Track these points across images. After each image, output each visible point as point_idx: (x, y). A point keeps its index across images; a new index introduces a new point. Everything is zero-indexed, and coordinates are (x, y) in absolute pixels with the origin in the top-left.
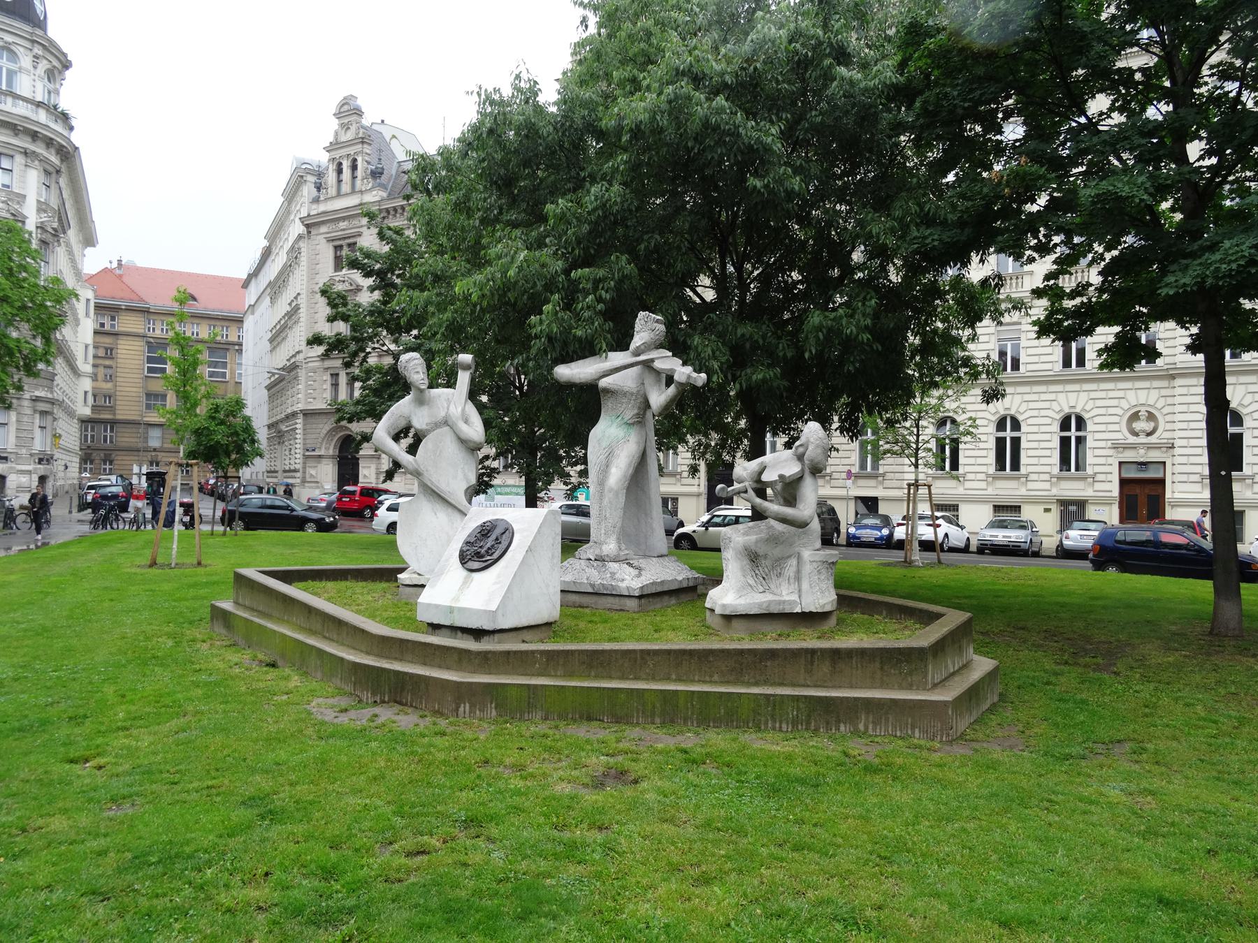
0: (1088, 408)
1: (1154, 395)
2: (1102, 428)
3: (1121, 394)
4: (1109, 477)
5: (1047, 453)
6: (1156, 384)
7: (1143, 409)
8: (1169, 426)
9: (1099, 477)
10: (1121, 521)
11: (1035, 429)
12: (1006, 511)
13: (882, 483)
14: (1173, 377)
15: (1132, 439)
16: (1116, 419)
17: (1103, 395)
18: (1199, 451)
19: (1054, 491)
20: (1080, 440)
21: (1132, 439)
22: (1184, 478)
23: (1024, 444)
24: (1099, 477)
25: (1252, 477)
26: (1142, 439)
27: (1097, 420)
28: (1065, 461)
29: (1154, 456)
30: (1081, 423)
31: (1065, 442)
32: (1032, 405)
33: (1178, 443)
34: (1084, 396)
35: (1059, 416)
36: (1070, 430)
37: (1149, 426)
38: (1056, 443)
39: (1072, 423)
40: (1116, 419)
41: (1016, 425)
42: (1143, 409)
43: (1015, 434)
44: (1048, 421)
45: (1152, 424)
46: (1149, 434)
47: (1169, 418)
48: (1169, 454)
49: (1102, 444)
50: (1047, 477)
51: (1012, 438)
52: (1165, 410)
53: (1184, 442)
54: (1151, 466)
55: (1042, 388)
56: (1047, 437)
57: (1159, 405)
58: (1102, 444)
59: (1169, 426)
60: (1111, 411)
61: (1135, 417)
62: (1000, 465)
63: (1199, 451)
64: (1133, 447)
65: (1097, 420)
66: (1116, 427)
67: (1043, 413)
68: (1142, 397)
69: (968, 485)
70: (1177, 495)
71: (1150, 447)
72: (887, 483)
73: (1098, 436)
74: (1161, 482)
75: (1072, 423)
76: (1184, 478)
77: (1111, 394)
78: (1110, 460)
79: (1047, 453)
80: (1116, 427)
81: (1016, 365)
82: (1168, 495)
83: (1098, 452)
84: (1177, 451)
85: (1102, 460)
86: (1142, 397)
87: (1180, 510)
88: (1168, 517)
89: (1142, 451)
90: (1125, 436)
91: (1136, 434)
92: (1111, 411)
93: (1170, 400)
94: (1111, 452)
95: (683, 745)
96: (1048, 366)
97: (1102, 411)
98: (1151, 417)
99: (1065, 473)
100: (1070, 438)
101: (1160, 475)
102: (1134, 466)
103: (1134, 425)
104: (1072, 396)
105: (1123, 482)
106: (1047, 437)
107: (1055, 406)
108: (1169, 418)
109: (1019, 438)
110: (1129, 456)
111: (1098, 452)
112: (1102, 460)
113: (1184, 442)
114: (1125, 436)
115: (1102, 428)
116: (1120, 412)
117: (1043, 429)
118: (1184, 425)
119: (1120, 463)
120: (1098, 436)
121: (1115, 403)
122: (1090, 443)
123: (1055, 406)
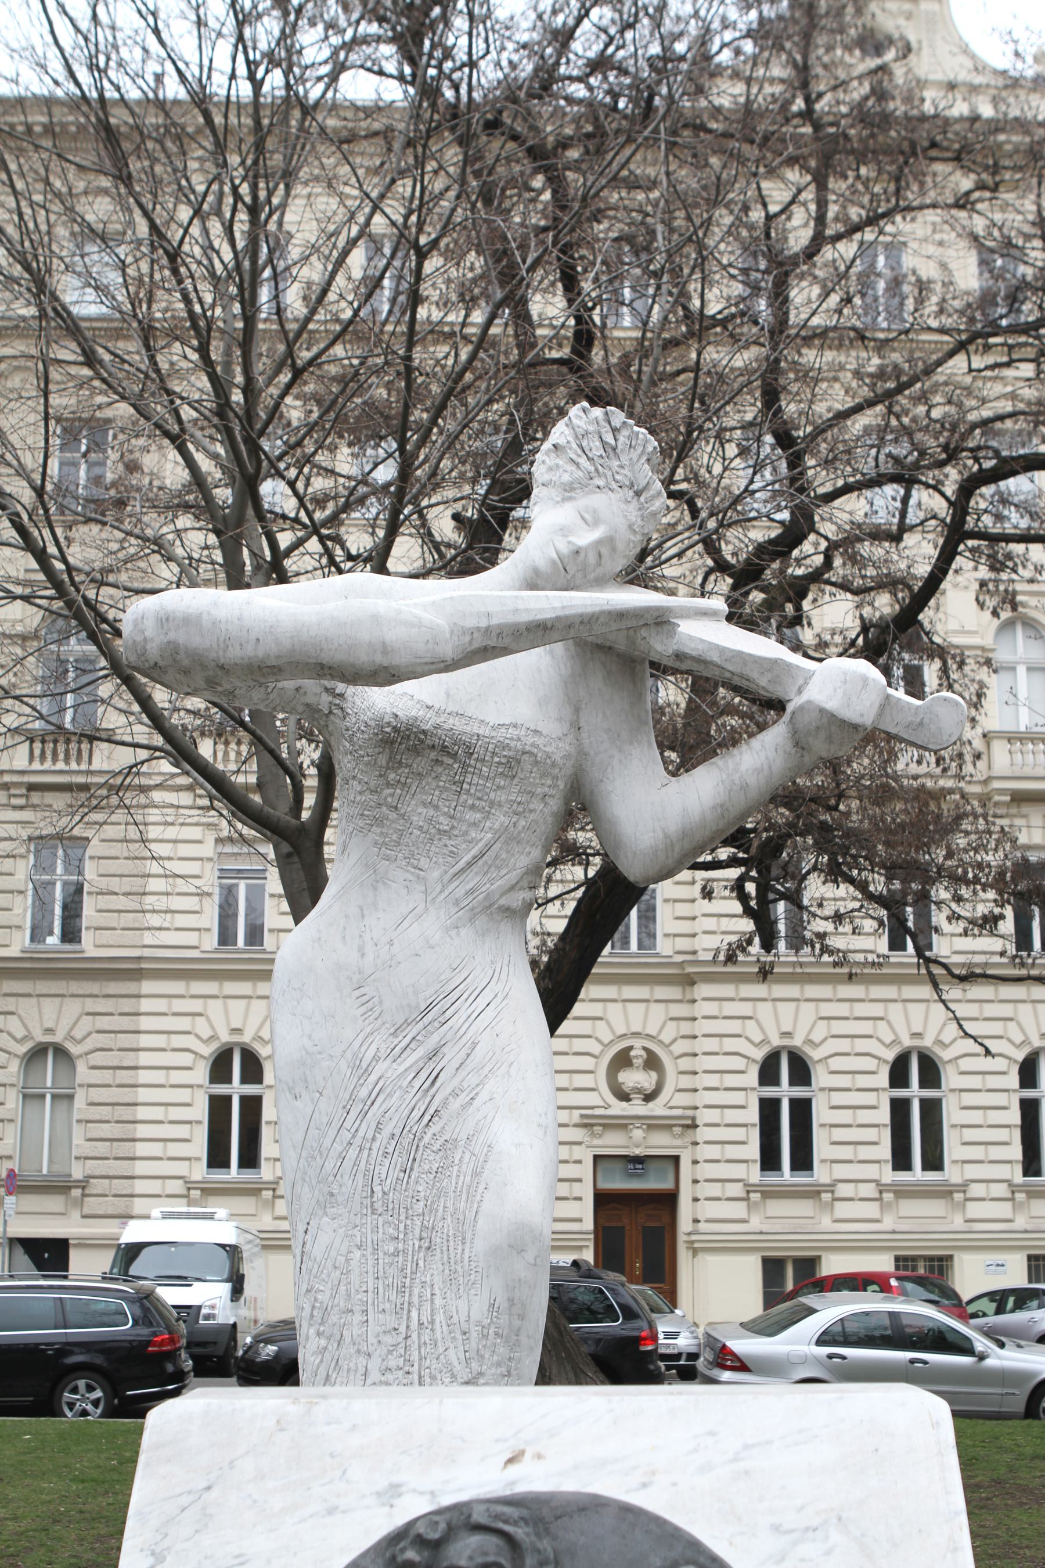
0: (816, 1037)
1: (658, 1012)
4: (577, 1189)
5: (182, 1131)
6: (663, 992)
7: (638, 1043)
8: (686, 1082)
11: (844, 1081)
13: (80, 1203)
14: (689, 981)
15: (619, 1108)
16: (587, 1063)
17: (843, 1009)
18: (1002, 1135)
21: (619, 1108)
22: (715, 1190)
23: (820, 1114)
25: (273, 1186)
26: (637, 1108)
27: (836, 1063)
29: (661, 1144)
32: (838, 1027)
33: (704, 1116)
34: (808, 1011)
35: (208, 1050)
36: (229, 1080)
37: (645, 1080)
38: (201, 1111)
39: (914, 1068)
40: (587, 1063)
41: (801, 1072)
42: (638, 1043)
43: (251, 1089)
44: (186, 1059)
45: (654, 1075)
46: (649, 1097)
47: (685, 1064)
48: (688, 1139)
51: (244, 1099)
53: (713, 1116)
54: (652, 1166)
55: (176, 987)
56: (184, 1095)
59: (686, 1082)
61: (622, 1060)
63: (1002, 1135)
64: (620, 1124)
65: (836, 1063)
66: (586, 1081)
67: (178, 1041)
69: (842, 1210)
71: (654, 1125)
72: (92, 1205)
74: (669, 1200)
75: (914, 1068)
76: (715, 1190)
78: (578, 1152)
79: (182, 1131)
80: (586, 1081)
82: (684, 1224)
84: (703, 1134)
89: (638, 1134)
91: (623, 1096)
93: (686, 1028)
94: (578, 1134)
96: (191, 938)
97: (844, 1045)
98: (652, 1062)
99: (219, 1176)
100: (228, 1099)
101: (668, 1185)
102: (618, 1166)
104: (237, 1007)
105: (603, 1200)
106: (184, 1095)
107: (202, 1028)
108: (685, 1064)
110: (614, 1143)
113: (713, 1116)
116: (595, 1048)
117: (176, 1077)
118: (713, 1080)
119: (596, 1158)
123: (202, 1028)
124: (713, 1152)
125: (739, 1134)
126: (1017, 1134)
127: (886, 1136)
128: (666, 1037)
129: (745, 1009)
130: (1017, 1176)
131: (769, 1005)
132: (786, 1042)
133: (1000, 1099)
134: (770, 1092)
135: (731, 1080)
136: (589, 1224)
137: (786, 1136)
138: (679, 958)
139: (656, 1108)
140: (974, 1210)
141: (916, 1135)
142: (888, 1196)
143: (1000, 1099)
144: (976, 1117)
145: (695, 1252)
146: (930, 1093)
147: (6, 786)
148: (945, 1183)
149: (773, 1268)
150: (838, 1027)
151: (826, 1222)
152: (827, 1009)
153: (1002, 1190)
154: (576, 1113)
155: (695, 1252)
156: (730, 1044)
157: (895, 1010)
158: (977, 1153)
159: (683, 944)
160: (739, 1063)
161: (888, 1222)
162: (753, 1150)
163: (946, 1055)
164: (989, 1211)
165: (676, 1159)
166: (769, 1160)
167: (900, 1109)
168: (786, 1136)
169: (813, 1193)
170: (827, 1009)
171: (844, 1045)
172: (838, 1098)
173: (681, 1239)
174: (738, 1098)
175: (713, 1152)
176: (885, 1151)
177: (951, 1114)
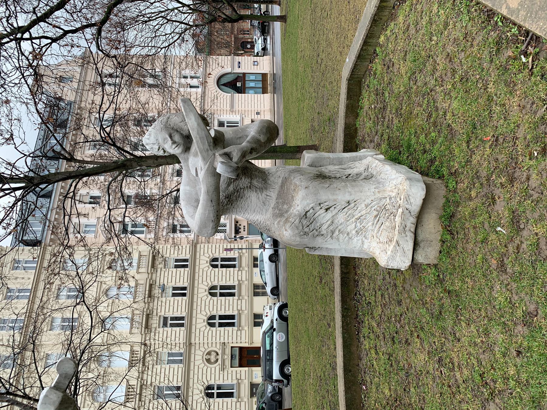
1: (198, 352)
2: (213, 376)
3: (196, 368)
4: (239, 372)
6: (193, 351)
7: (205, 357)
8: (214, 345)
9: (238, 377)
10: (260, 366)
12: (258, 290)
14: (190, 344)
15: (220, 361)
16: (209, 370)
18: (228, 272)
19: (246, 400)
20: (219, 388)
21: (220, 361)
22: (239, 338)
23: (222, 313)
24: (238, 377)
26: (220, 357)
28: (230, 395)
29: (228, 351)
30: (210, 387)
31: (220, 395)
32: (203, 309)
33: (222, 341)
34: (200, 286)
35: (208, 327)
36: (215, 323)
37: (214, 354)
38: (220, 400)
39: (212, 291)
40: (209, 370)
41: (212, 317)
44: (211, 301)
45: (213, 353)
46: (218, 354)
47: (210, 345)
49: (221, 376)
50: (238, 404)
52: (206, 346)
53: (222, 338)
54: (233, 353)
57: (203, 350)
58: (221, 376)
59: (214, 345)
60: (205, 372)
61: (208, 361)
62: (233, 325)
63: (228, 272)
64: (223, 361)
65: (211, 309)
68: (199, 357)
70: (247, 341)
71: (224, 353)
73: (217, 378)
74: (241, 348)
76: (239, 338)
77: (196, 372)
78: (230, 372)
81: (178, 388)
82: (246, 345)
83: (225, 378)
84: (226, 341)
85: (230, 376)
86: (199, 357)
87: (254, 339)
88: (259, 345)
89: (226, 357)
90: (217, 366)
91: (217, 360)
92: (205, 372)
93: (201, 345)
95: (395, 64)
96: (180, 370)
97: (207, 307)
98: (209, 353)
100: (219, 323)
101: (238, 349)
102: (233, 361)
103: (212, 361)
104: (197, 357)
105: (241, 366)
108: (210, 345)
109: (220, 316)
110: (228, 363)
111: (225, 378)
112: (230, 376)
113: (222, 338)
114: (217, 366)
115: (213, 376)
116: (206, 367)
119: (231, 367)
120: (217, 378)
121: (200, 370)
122: (221, 382)
123: (202, 329)
124: (230, 338)
125: (227, 301)
126: (228, 269)
127: (227, 328)
128: (203, 350)
129: (198, 331)
130: (235, 328)
131: (197, 325)
132: (207, 291)
133: (220, 272)
134: (217, 325)
135: (215, 303)
136: (246, 369)
137: (227, 321)
138: (185, 347)
139: (220, 352)
140: (244, 279)
141: (227, 291)
142: (241, 298)
143: (220, 272)
144: (223, 307)
145: (252, 343)
146: (220, 260)
147: (139, 407)
148: (238, 285)
149: (256, 294)
150: (206, 251)
151: (246, 312)
152: (202, 254)
153: (239, 302)
154: (221, 372)
155: (252, 343)
156: (206, 335)
157: (201, 267)
158: (231, 307)
159: (182, 346)
160: (210, 332)
161: (246, 328)
162: (230, 329)
163: (209, 314)
164: (244, 275)
165: (232, 347)
166: (233, 295)
167: (223, 266)
168: (227, 321)
169: (240, 315)
170: (199, 311)
171: (207, 307)
172: (219, 309)
173: (249, 346)
174: (219, 301)
175: (230, 338)
176: (231, 298)
177: (223, 283)
